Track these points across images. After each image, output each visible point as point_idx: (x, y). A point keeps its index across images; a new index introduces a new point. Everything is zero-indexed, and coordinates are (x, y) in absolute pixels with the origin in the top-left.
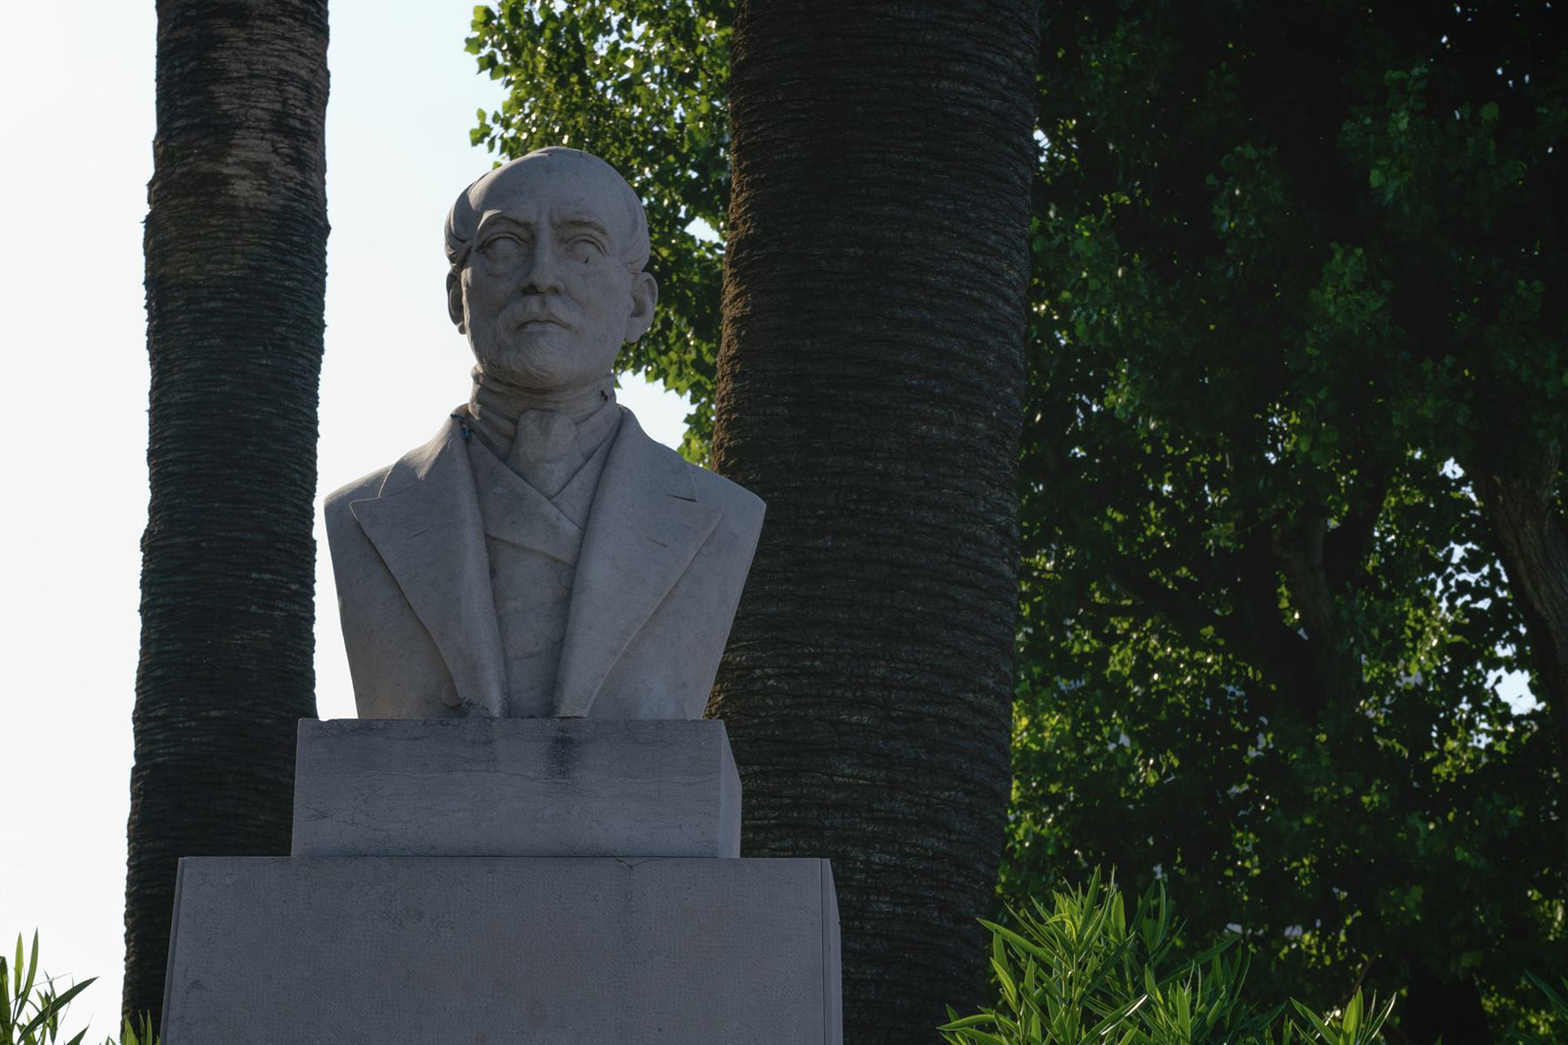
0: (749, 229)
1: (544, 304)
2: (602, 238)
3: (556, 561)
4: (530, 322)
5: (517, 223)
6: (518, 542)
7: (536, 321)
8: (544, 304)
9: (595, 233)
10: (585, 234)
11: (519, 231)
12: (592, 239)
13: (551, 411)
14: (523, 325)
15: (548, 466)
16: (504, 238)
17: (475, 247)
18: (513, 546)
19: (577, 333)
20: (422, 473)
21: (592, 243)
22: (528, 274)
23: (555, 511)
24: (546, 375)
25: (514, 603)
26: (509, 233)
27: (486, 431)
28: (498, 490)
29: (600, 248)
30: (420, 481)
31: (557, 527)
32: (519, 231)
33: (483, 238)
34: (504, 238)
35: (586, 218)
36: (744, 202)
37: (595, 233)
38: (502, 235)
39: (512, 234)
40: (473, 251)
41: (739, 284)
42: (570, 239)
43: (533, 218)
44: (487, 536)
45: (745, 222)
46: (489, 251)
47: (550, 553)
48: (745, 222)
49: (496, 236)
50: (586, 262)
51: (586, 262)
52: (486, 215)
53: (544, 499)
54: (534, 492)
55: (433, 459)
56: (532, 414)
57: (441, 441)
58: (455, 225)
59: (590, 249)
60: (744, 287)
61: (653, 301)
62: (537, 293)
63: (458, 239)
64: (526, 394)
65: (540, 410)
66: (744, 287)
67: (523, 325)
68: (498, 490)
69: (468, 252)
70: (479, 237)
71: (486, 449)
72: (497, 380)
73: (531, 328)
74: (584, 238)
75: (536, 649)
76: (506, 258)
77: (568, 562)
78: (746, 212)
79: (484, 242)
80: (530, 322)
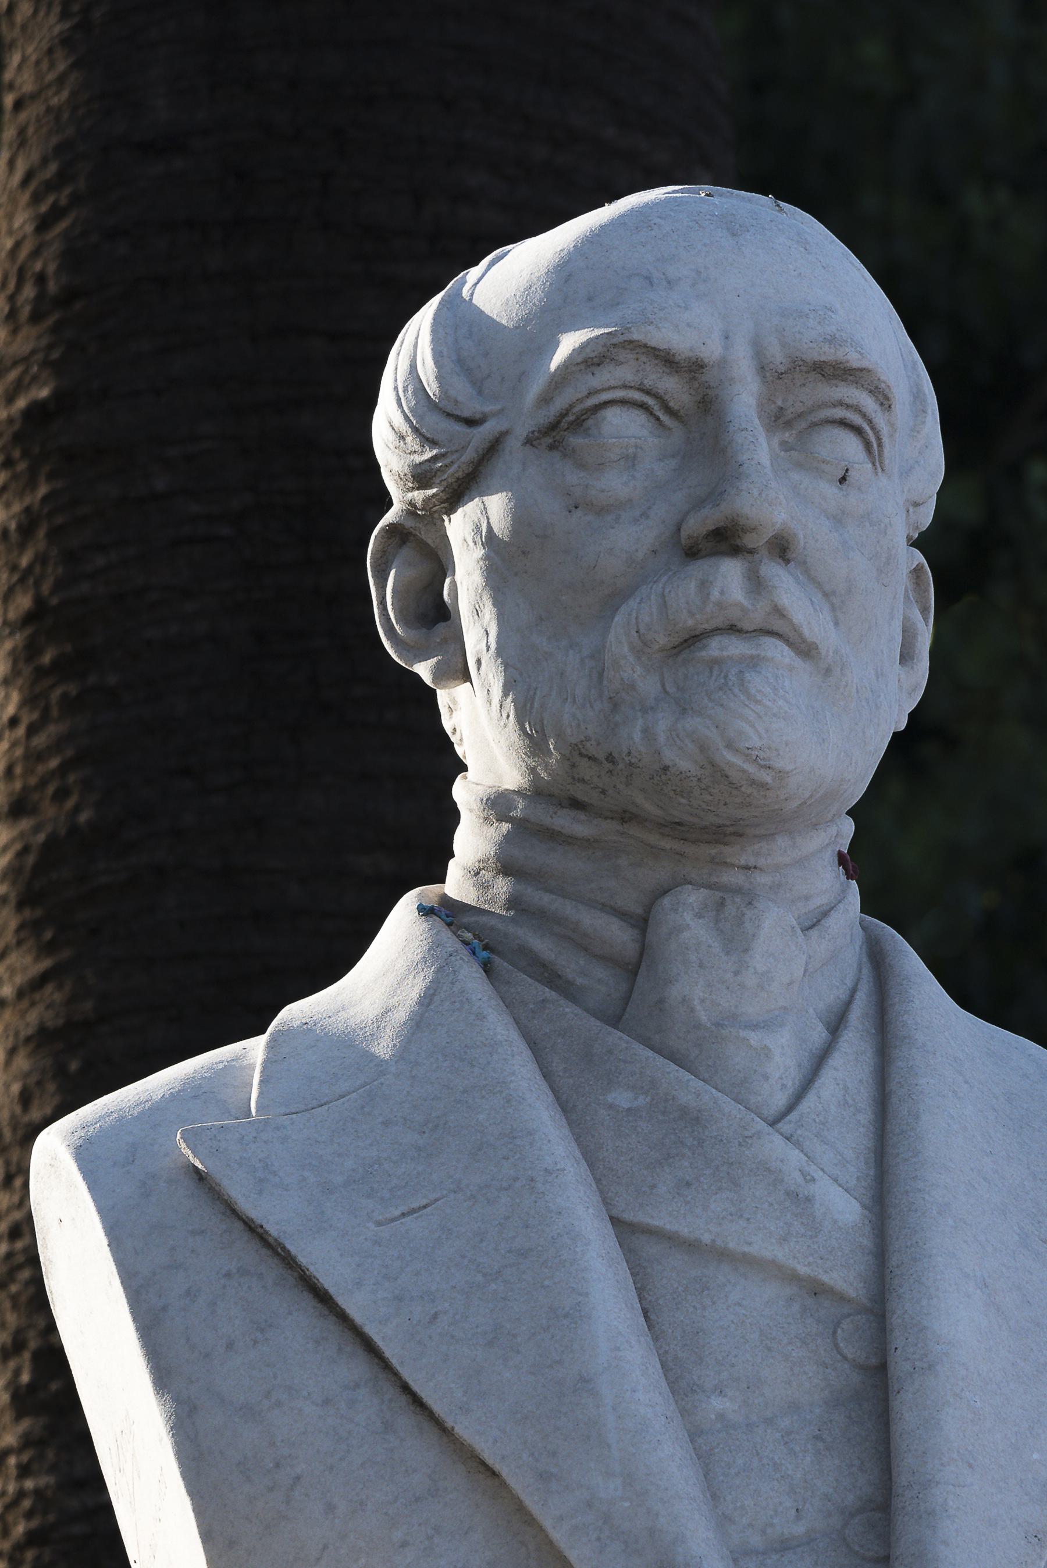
0: (77, 809)
1: (756, 584)
2: (880, 420)
3: (817, 1290)
4: (717, 631)
5: (667, 360)
6: (706, 1238)
7: (733, 629)
8: (756, 584)
9: (869, 404)
10: (840, 404)
11: (671, 385)
12: (857, 420)
13: (738, 891)
14: (693, 640)
15: (754, 1038)
16: (623, 402)
17: (522, 431)
18: (691, 1247)
19: (828, 671)
20: (383, 1048)
21: (858, 430)
22: (714, 495)
23: (795, 1156)
24: (766, 777)
25: (717, 1403)
26: (641, 389)
27: (542, 945)
28: (622, 1098)
29: (872, 448)
30: (380, 1064)
31: (809, 1200)
32: (671, 385)
33: (560, 403)
34: (623, 402)
35: (854, 360)
36: (56, 747)
37: (869, 404)
38: (619, 394)
39: (648, 392)
40: (514, 445)
41: (47, 949)
42: (800, 415)
43: (712, 350)
44: (615, 1221)
45: (61, 795)
46: (575, 441)
47: (803, 1270)
48: (61, 795)
49: (606, 396)
50: (843, 480)
51: (843, 480)
52: (569, 343)
53: (760, 1125)
54: (728, 1105)
55: (401, 1015)
56: (693, 897)
57: (413, 968)
58: (439, 378)
59: (851, 447)
60: (66, 954)
61: (926, 620)
62: (736, 551)
63: (459, 419)
64: (667, 844)
65: (709, 886)
66: (66, 954)
67: (693, 640)
68: (622, 1098)
69: (493, 448)
70: (545, 399)
71: (549, 994)
72: (576, 804)
73: (716, 647)
74: (839, 413)
75: (799, 1529)
76: (630, 460)
77: (852, 1293)
78: (63, 770)
79: (564, 414)
80: (717, 631)
